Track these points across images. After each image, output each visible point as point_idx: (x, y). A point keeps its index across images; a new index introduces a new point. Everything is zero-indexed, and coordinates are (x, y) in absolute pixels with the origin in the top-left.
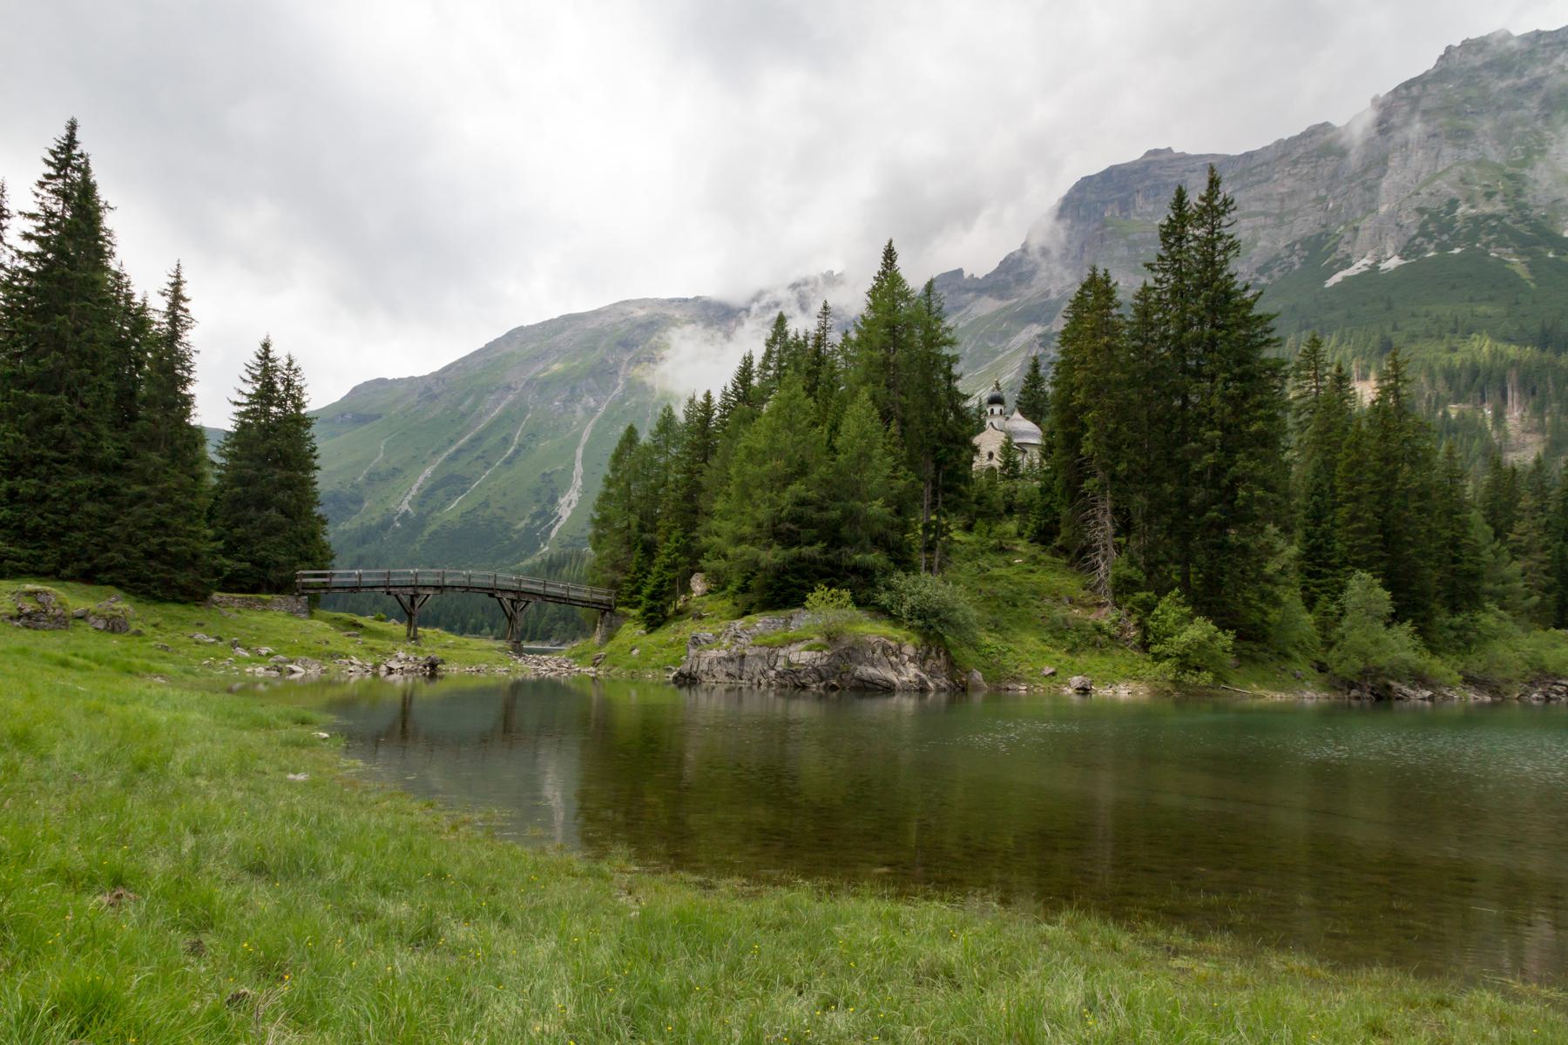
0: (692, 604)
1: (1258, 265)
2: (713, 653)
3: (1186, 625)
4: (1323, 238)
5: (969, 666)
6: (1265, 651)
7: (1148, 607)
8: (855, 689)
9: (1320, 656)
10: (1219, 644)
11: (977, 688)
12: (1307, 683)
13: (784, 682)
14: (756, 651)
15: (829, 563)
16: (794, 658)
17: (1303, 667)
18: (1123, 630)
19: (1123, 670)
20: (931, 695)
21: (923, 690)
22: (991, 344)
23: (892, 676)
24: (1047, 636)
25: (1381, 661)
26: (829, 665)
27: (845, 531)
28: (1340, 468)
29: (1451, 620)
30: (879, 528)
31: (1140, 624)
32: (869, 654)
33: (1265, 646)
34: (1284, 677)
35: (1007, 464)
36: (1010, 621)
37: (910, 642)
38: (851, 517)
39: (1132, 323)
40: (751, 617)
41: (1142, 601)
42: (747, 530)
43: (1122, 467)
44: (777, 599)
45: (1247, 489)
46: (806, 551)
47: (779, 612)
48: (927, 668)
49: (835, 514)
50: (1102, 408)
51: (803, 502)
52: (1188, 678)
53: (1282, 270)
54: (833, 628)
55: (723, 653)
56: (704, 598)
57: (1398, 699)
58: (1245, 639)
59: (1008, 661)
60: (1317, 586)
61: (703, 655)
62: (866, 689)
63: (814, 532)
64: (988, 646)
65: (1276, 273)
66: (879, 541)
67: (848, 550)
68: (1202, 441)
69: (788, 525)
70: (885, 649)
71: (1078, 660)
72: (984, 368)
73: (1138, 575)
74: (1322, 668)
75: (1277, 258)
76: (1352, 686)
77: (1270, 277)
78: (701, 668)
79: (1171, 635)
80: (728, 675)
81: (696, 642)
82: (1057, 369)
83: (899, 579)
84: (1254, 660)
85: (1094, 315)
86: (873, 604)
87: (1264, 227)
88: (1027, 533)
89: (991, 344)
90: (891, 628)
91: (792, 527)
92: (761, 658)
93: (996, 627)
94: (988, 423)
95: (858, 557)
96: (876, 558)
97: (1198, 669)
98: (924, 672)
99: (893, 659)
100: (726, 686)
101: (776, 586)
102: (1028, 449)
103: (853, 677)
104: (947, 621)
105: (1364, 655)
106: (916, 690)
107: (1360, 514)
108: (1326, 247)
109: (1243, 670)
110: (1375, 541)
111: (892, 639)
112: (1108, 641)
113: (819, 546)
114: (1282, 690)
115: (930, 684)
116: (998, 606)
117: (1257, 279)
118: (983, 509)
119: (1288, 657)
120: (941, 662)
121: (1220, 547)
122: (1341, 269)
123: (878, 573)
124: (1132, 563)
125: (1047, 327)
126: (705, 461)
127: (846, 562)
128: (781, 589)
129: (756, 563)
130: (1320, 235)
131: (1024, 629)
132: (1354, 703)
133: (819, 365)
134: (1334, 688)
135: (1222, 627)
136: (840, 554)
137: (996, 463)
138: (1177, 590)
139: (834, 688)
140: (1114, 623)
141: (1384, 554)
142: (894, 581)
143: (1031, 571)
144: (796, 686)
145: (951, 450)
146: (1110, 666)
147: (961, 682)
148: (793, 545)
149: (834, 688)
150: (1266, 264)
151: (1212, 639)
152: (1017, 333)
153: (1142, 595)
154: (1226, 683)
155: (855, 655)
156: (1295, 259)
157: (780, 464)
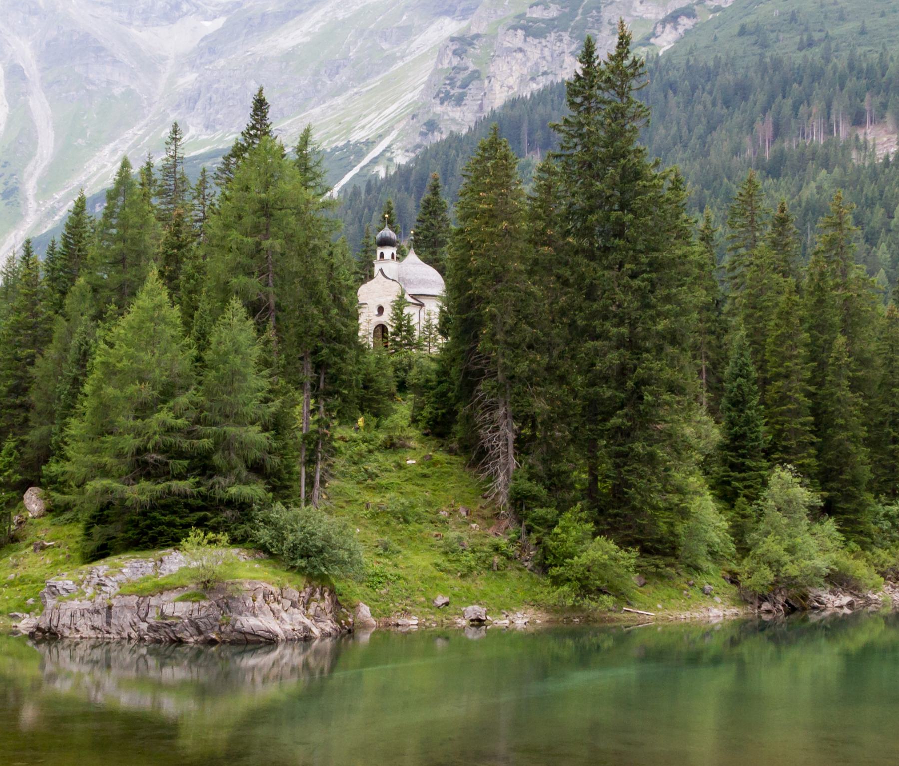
2: (75, 604)
5: (355, 599)
9: (734, 567)
12: (718, 599)
13: (157, 636)
16: (168, 610)
17: (714, 579)
20: (316, 643)
22: (385, 46)
23: (275, 626)
24: (440, 560)
25: (792, 570)
26: (207, 617)
27: (217, 459)
29: (887, 508)
30: (255, 454)
32: (249, 602)
33: (673, 560)
34: (691, 593)
36: (400, 542)
38: (223, 443)
40: (113, 560)
44: (145, 539)
47: (147, 553)
48: (311, 611)
55: (87, 605)
57: (814, 608)
60: (737, 480)
66: (257, 468)
69: (155, 456)
72: (374, 82)
74: (734, 579)
76: (763, 599)
78: (62, 621)
80: (94, 628)
82: (427, 423)
84: (661, 577)
85: (492, 194)
89: (385, 46)
92: (131, 608)
94: (376, 269)
96: (256, 490)
97: (601, 591)
98: (308, 616)
99: (275, 606)
100: (92, 642)
101: (142, 524)
102: (423, 301)
103: (234, 630)
105: (775, 564)
109: (650, 588)
115: (314, 629)
116: (387, 524)
119: (698, 569)
120: (326, 603)
121: (625, 455)
123: (255, 507)
125: (465, 24)
127: (219, 493)
128: (149, 527)
133: (180, 247)
136: (212, 487)
137: (386, 318)
141: (815, 439)
145: (333, 350)
147: (347, 623)
152: (421, 30)
154: (629, 604)
155: (234, 604)
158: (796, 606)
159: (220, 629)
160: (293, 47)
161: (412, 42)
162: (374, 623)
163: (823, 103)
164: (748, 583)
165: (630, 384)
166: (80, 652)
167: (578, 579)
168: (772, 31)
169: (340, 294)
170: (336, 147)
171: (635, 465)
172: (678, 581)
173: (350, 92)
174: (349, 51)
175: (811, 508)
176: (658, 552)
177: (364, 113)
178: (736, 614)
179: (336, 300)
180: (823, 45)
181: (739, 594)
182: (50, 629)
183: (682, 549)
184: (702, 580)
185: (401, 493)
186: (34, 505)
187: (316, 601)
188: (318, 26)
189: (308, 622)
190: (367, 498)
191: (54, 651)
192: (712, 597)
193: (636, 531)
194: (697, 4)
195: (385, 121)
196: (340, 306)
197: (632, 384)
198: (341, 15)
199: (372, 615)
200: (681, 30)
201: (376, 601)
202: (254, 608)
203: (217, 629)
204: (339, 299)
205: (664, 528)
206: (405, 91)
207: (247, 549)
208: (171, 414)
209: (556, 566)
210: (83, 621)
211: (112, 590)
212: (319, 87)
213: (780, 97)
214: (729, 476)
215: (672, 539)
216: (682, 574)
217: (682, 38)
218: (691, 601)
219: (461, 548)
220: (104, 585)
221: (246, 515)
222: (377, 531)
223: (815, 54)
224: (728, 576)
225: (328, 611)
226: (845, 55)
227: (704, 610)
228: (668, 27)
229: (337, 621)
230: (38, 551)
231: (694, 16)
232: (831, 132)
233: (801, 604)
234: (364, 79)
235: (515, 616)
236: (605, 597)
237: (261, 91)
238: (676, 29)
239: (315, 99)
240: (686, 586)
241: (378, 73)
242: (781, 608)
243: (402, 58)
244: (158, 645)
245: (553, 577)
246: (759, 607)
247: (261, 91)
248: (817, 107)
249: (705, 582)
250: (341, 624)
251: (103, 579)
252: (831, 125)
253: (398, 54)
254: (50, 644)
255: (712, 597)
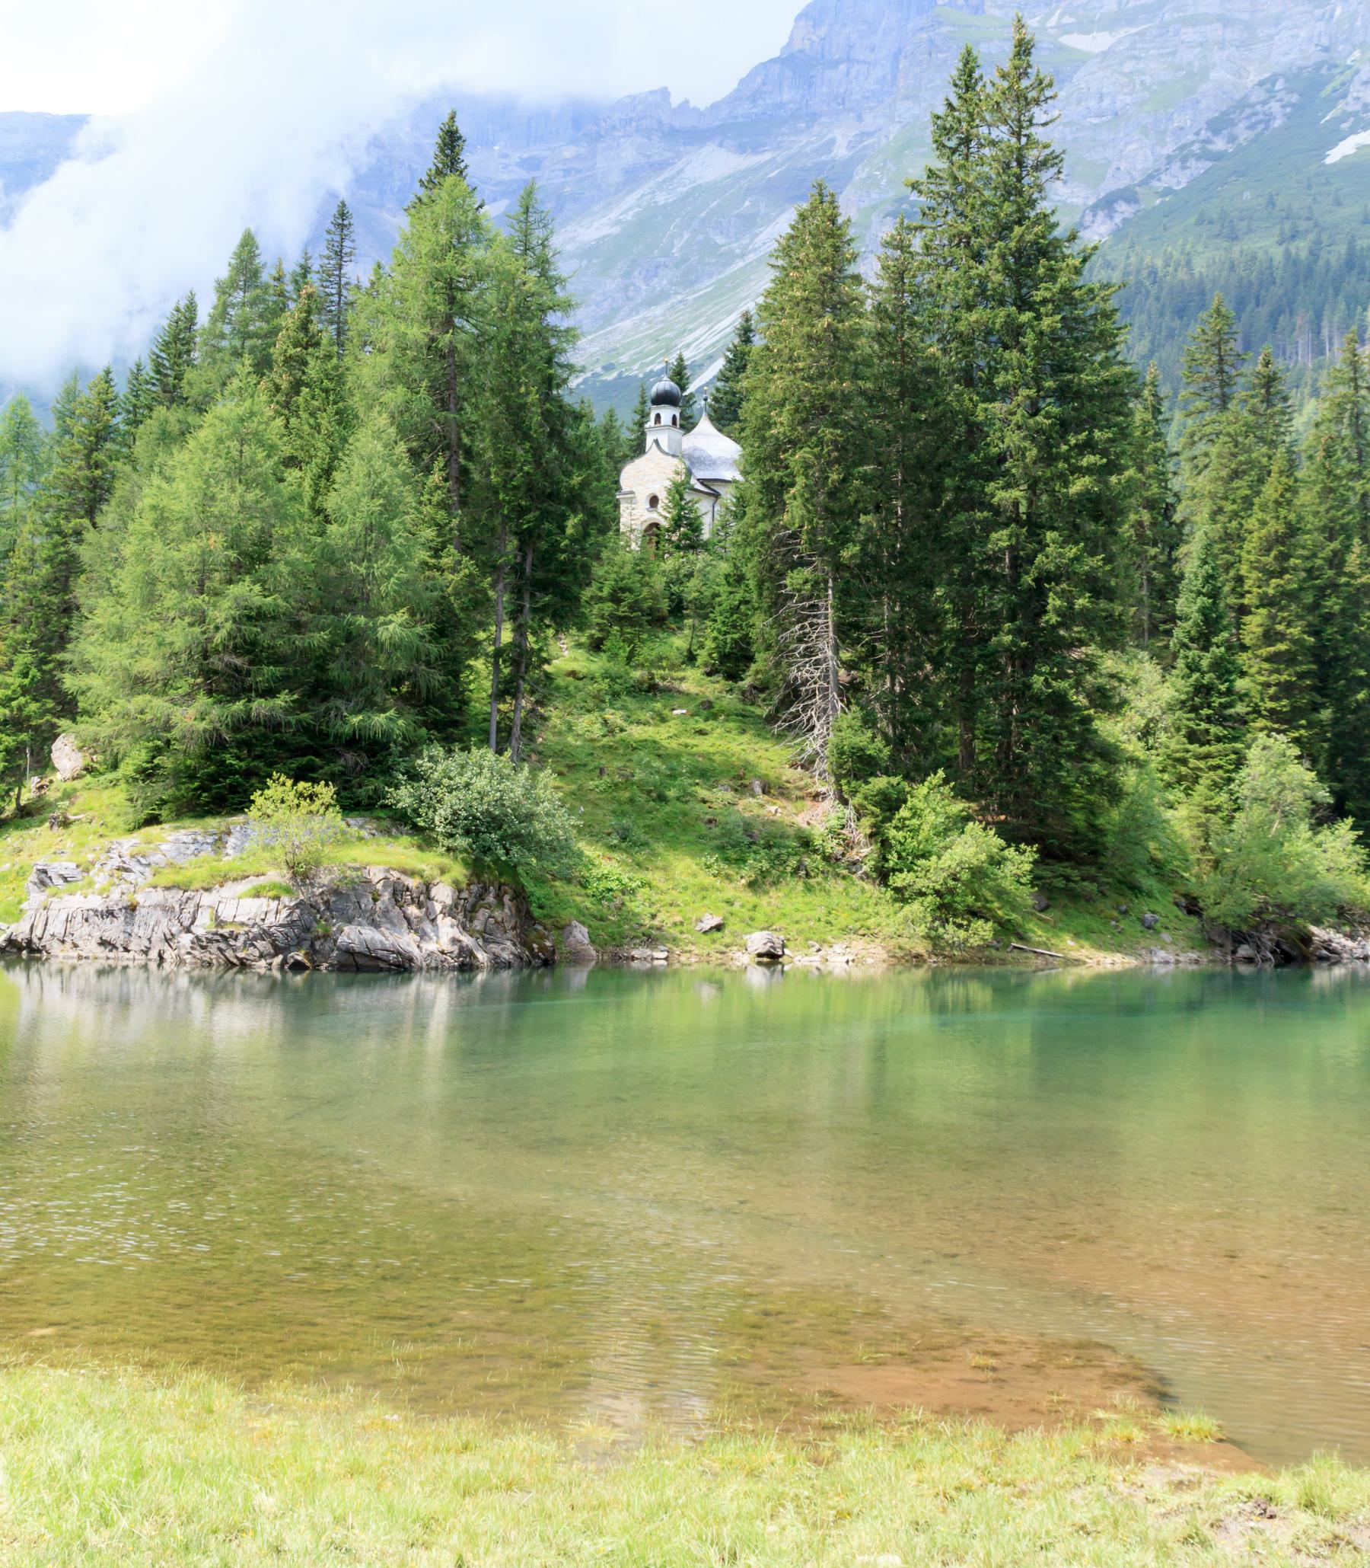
0: (51, 795)
1: (1211, 115)
3: (954, 836)
4: (1324, 71)
5: (565, 915)
6: (1092, 879)
7: (890, 804)
8: (341, 968)
10: (1009, 869)
11: (577, 958)
12: (1166, 936)
13: (207, 957)
14: (158, 896)
15: (306, 729)
17: (1162, 906)
18: (849, 845)
19: (844, 919)
20: (480, 977)
21: (466, 966)
22: (720, 240)
23: (407, 941)
28: (1252, 544)
31: (876, 834)
32: (367, 902)
33: (1093, 870)
34: (1122, 925)
35: (677, 523)
37: (447, 878)
39: (879, 290)
41: (881, 792)
42: (150, 665)
43: (849, 552)
45: (1062, 595)
46: (260, 706)
48: (478, 925)
49: (319, 638)
50: (820, 442)
51: (257, 616)
52: (951, 933)
53: (1251, 127)
54: (301, 855)
55: (97, 902)
56: (78, 784)
57: (1322, 958)
58: (1059, 859)
59: (637, 905)
60: (1199, 757)
61: (56, 904)
62: (359, 969)
63: (278, 671)
64: (606, 877)
65: (1243, 134)
67: (339, 703)
68: (991, 507)
70: (398, 892)
71: (764, 900)
72: (706, 286)
73: (878, 748)
75: (1243, 104)
76: (1239, 938)
77: (1232, 139)
78: (50, 930)
79: (925, 855)
80: (104, 943)
81: (43, 879)
83: (436, 761)
84: (1074, 896)
86: (384, 807)
87: (1222, 45)
88: (702, 656)
90: (414, 851)
91: (238, 661)
92: (167, 909)
93: (626, 841)
95: (356, 720)
97: (975, 914)
99: (413, 910)
104: (517, 836)
106: (453, 969)
107: (1280, 628)
108: (1329, 88)
110: (1301, 676)
111: (412, 873)
112: (822, 865)
113: (283, 700)
114: (1118, 948)
116: (632, 801)
117: (1208, 141)
118: (623, 610)
122: (1353, 131)
124: (869, 721)
126: (91, 513)
129: (168, 727)
130: (1318, 66)
131: (674, 844)
132: (1244, 969)
134: (1210, 943)
135: (1012, 836)
136: (327, 712)
138: (941, 773)
139: (298, 967)
140: (835, 833)
142: (423, 764)
143: (701, 733)
144: (230, 965)
146: (821, 912)
147: (542, 948)
148: (236, 697)
149: (298, 967)
150: (1224, 114)
151: (997, 862)
153: (880, 782)
156: (1275, 107)
157: (216, 541)
158: (1294, 953)
159: (312, 946)
160: (598, 240)
161: (757, 235)
162: (594, 953)
163: (1311, 313)
164: (1214, 912)
165: (1028, 580)
166: (76, 982)
167: (938, 893)
168: (1241, 219)
169: (563, 425)
170: (651, 371)
171: (1032, 712)
172: (1101, 905)
173: (672, 301)
174: (672, 247)
175: (1316, 805)
176: (1068, 857)
177: (690, 327)
178: (1197, 962)
179: (555, 434)
180: (1311, 237)
181: (1202, 930)
182: (30, 942)
183: (1109, 854)
184: (1145, 908)
185: (659, 756)
186: (66, 761)
187: (489, 906)
188: (631, 213)
189: (467, 940)
190: (603, 762)
191: (34, 977)
192: (1157, 932)
193: (1034, 821)
194: (1139, 185)
195: (717, 337)
196: (563, 446)
197: (1029, 580)
198: (662, 198)
199: (592, 942)
200: (1118, 219)
201: (602, 919)
202: (373, 912)
203: (307, 943)
204: (560, 433)
205: (1079, 819)
206: (745, 298)
207: (378, 818)
208: (257, 588)
209: (901, 871)
210: (86, 928)
211: (140, 880)
212: (631, 294)
213: (1252, 304)
214: (1188, 751)
215: (1092, 836)
216: (1108, 893)
217: (1119, 230)
218: (1123, 938)
219: (747, 840)
220: (127, 870)
221: (379, 762)
222: (614, 812)
223: (1301, 248)
224: (1183, 901)
225: (508, 925)
226: (1343, 249)
227: (1144, 952)
228: (1101, 215)
229: (525, 944)
230: (55, 828)
231: (1136, 201)
232: (1322, 352)
233: (1301, 950)
234: (691, 283)
235: (830, 951)
236: (981, 922)
237: (452, 118)
238: (1111, 218)
239: (626, 309)
240: (1115, 914)
241: (710, 276)
242: (1270, 955)
243: (743, 255)
244: (206, 972)
245: (897, 890)
246: (1234, 952)
247: (452, 118)
248: (1302, 318)
249: (1146, 909)
250: (531, 950)
251: (126, 859)
252: (1322, 342)
253: (738, 251)
254: (28, 968)
255: (1157, 932)
